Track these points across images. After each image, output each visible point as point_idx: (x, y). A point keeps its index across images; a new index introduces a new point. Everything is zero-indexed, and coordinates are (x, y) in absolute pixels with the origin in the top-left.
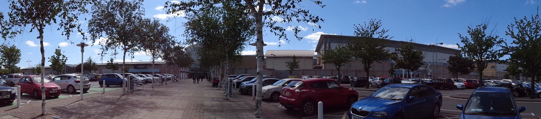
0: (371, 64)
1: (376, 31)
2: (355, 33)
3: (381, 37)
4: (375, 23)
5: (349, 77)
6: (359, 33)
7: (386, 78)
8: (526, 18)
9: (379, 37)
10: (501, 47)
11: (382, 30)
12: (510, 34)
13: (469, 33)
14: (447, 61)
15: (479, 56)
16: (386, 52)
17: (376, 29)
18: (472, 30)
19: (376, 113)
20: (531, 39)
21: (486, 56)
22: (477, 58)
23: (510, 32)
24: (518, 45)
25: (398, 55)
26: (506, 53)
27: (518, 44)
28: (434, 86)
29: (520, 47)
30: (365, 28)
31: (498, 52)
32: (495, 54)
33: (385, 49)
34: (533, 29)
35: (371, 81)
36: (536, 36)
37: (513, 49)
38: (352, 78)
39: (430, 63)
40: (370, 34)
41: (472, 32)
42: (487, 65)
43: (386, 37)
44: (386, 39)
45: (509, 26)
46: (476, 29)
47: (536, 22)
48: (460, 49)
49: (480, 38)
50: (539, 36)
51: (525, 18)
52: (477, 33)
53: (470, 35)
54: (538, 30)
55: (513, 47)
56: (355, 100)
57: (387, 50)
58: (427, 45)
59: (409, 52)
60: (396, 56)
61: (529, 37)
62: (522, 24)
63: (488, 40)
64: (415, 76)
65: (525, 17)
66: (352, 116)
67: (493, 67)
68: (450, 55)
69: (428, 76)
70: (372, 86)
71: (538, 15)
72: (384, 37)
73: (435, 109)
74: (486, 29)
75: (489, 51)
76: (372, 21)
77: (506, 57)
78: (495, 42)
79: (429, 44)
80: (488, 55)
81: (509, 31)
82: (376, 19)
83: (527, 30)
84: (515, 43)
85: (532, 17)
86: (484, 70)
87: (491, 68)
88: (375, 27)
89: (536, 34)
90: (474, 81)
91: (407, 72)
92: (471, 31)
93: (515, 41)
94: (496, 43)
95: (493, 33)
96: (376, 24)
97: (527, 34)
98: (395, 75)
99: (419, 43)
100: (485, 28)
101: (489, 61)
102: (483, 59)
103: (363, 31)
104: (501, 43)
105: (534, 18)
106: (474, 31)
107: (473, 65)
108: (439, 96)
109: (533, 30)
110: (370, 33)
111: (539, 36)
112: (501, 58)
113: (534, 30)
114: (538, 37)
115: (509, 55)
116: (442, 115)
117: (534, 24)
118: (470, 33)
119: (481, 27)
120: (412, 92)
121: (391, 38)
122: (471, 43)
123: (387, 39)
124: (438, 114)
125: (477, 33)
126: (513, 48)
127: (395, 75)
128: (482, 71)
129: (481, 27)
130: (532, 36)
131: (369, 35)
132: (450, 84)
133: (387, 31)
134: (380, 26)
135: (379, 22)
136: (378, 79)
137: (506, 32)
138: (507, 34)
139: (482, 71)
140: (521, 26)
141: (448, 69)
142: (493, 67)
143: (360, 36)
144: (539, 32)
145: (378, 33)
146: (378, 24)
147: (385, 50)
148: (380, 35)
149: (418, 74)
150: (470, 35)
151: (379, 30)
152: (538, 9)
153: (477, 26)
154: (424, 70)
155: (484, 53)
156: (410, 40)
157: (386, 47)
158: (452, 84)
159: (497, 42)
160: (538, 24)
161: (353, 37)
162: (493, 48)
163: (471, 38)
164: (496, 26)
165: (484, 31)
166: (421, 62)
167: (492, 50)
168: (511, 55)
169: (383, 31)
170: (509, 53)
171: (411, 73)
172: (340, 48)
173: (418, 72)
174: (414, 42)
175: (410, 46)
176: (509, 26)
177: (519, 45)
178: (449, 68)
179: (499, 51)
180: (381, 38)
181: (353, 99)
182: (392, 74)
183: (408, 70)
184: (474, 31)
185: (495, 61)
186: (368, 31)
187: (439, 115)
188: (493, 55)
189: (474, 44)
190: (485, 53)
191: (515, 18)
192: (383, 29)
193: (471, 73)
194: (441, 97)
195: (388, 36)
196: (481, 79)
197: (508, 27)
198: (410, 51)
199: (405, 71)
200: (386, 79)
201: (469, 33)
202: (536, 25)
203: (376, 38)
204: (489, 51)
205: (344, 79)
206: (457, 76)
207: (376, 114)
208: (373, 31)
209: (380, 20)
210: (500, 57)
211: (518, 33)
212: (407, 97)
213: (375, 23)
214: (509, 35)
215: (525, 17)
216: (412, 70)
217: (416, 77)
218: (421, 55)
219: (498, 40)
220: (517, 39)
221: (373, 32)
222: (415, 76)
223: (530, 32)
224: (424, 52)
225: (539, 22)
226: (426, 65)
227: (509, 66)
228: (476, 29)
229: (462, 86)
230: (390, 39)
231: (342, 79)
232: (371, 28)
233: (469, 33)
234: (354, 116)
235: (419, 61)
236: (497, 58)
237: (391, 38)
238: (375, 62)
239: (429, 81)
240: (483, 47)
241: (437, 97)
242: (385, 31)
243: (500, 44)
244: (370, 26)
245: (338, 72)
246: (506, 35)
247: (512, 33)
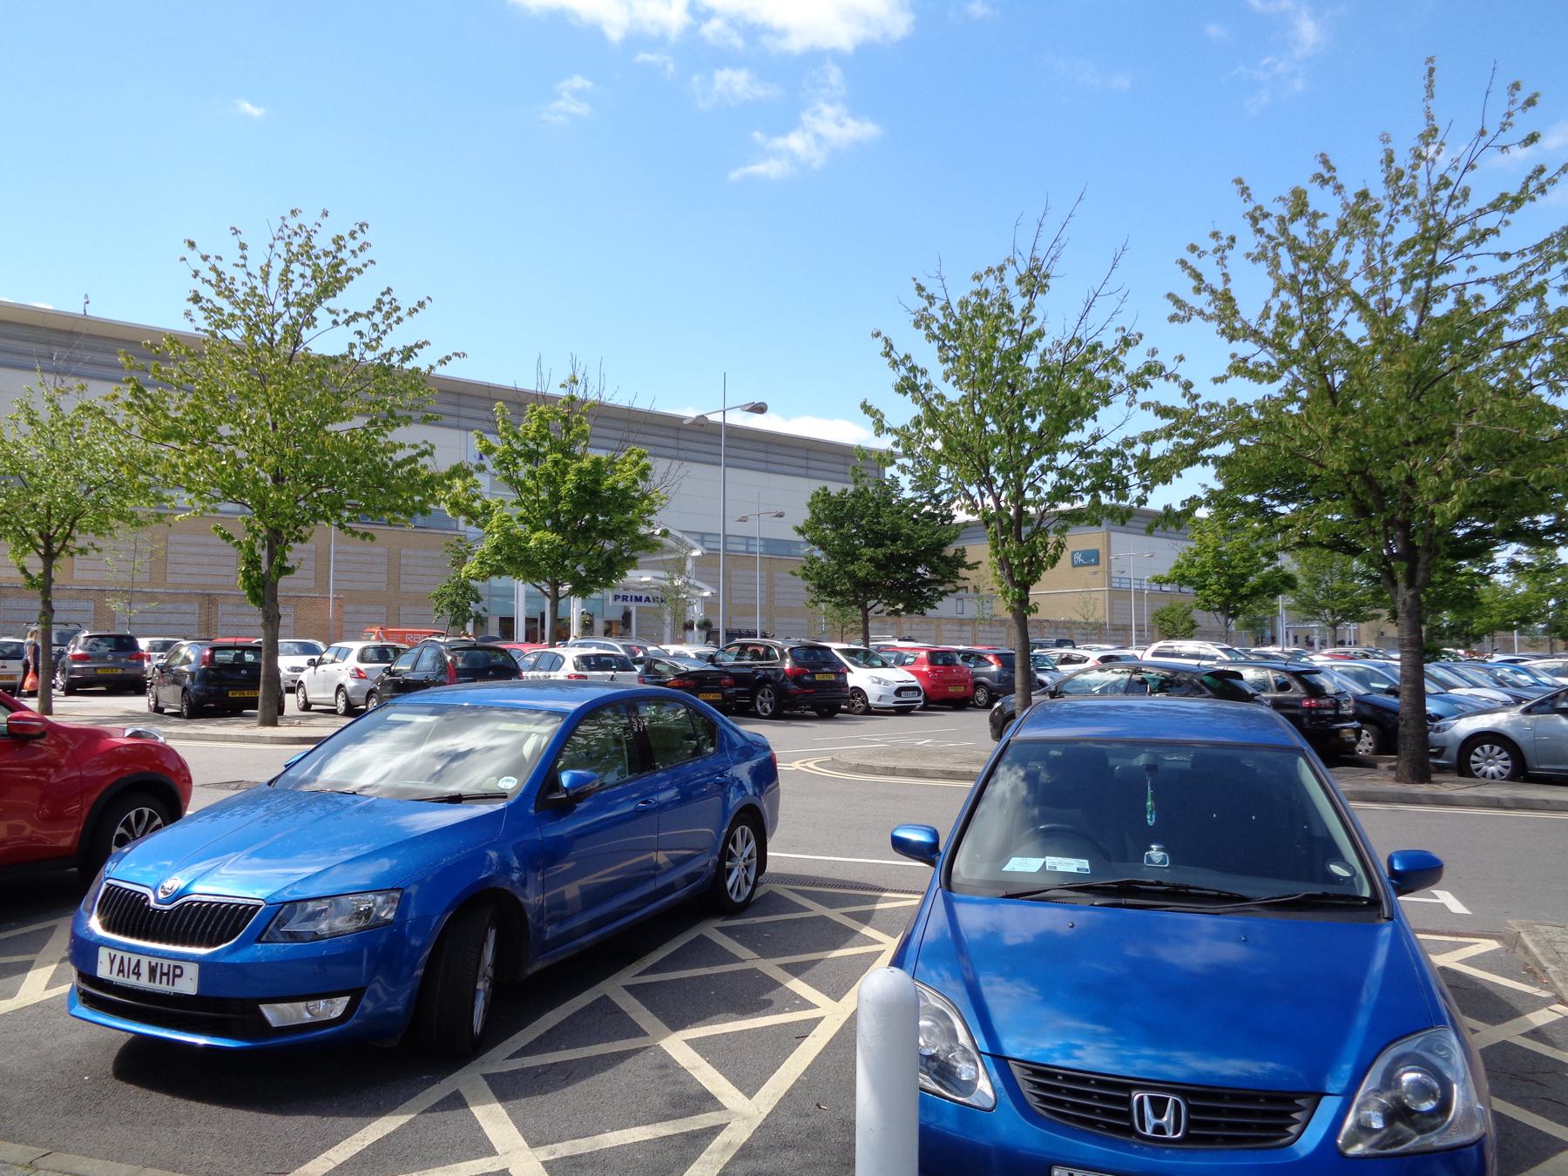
0: (297, 545)
1: (329, 303)
2: (194, 308)
3: (368, 346)
4: (322, 242)
5: (143, 643)
6: (228, 308)
7: (414, 646)
8: (1331, 168)
9: (352, 346)
10: (1151, 412)
11: (380, 301)
12: (1201, 313)
13: (928, 327)
14: (801, 525)
15: (1002, 489)
16: (413, 459)
17: (326, 291)
18: (942, 309)
19: (311, 906)
20: (1383, 321)
21: (1054, 487)
22: (989, 501)
23: (1206, 296)
24: (1275, 389)
25: (476, 485)
26: (1191, 457)
27: (1273, 378)
28: (717, 697)
29: (1291, 396)
30: (240, 275)
31: (1138, 449)
32: (1115, 462)
33: (398, 435)
34: (1400, 253)
35: (302, 670)
36: (1424, 301)
37: (1237, 420)
38: (166, 647)
39: (702, 537)
40: (285, 326)
41: (942, 321)
42: (1060, 546)
43: (408, 353)
44: (408, 365)
45: (1193, 248)
46: (974, 299)
47: (1422, 193)
48: (885, 443)
49: (1006, 356)
50: (1452, 296)
51: (1321, 169)
52: (979, 322)
53: (935, 345)
54: (1442, 256)
55: (1240, 403)
56: (159, 821)
57: (415, 446)
58: (680, 419)
59: (556, 463)
60: (465, 489)
61: (1372, 319)
62: (1299, 229)
63: (1066, 367)
64: (599, 625)
65: (1326, 162)
66: (104, 954)
67: (1091, 558)
68: (816, 485)
69: (689, 626)
70: (307, 706)
71: (1433, 131)
72: (393, 351)
73: (731, 856)
74: (1043, 288)
75: (1069, 448)
76: (293, 223)
77: (1197, 481)
78: (1117, 379)
79: (690, 413)
80: (1063, 472)
81: (1198, 290)
82: (326, 214)
83: (1344, 264)
84: (1255, 375)
85: (1389, 159)
86: (1045, 575)
87: (1074, 566)
88: (317, 271)
89: (1420, 284)
90: (967, 656)
91: (548, 602)
92: (939, 315)
93: (1245, 360)
94: (1125, 382)
95: (1097, 317)
96: (332, 248)
97: (1343, 288)
98: (480, 621)
99: (624, 403)
100: (1035, 282)
101: (1076, 517)
102: (1033, 503)
103: (229, 294)
104: (1146, 385)
105: (1403, 160)
106: (957, 312)
107: (949, 551)
108: (753, 763)
109: (1402, 259)
110: (286, 318)
111: (1452, 296)
112: (1159, 488)
113: (1406, 258)
114: (1439, 310)
115: (1211, 470)
116: (781, 889)
117: (1406, 210)
118: (935, 327)
119: (1011, 276)
120: (581, 741)
121: (442, 362)
122: (941, 397)
123: (417, 370)
124: (756, 885)
125: (979, 322)
126: (1239, 410)
127: (480, 621)
128: (1027, 589)
129: (1011, 276)
130: (1386, 304)
131: (278, 327)
132: (818, 677)
133: (413, 311)
134: (359, 271)
135: (353, 235)
136: (349, 651)
137: (1170, 296)
138: (1182, 312)
139: (1025, 586)
140: (1294, 245)
141: (806, 577)
142: (1091, 558)
143: (236, 334)
144: (1452, 268)
145: (347, 323)
146: (345, 254)
147: (402, 446)
148: (360, 333)
149: (618, 616)
150: (935, 345)
151: (355, 297)
152: (1430, 86)
153: (977, 277)
154: (663, 589)
155: (1036, 464)
156: (565, 376)
157: (408, 420)
158: (833, 678)
159: (1130, 378)
160: (1439, 208)
161: (175, 339)
162: (1095, 418)
163: (946, 360)
164: (1116, 260)
165: (1031, 306)
166: (643, 530)
167: (1095, 439)
168: (1221, 463)
169: (387, 309)
170: (1206, 452)
171: (575, 609)
172: (57, 409)
173: (619, 602)
174: (593, 396)
175: (566, 419)
176: (1193, 248)
177: (1280, 384)
178: (810, 572)
179: (1149, 438)
180: (369, 356)
181: (139, 816)
182: (460, 616)
183: (555, 585)
184: (957, 312)
185: (1123, 517)
186: (262, 302)
187: (760, 892)
188: (1105, 476)
189: (964, 399)
190: (1044, 460)
191: (1239, 181)
192: (389, 291)
193: (937, 604)
194: (766, 773)
195: (420, 346)
196: (1026, 646)
197: (1183, 263)
198: (567, 454)
199: (528, 596)
200: (416, 651)
201: (928, 327)
202: (1424, 219)
203: (334, 360)
204: (1069, 448)
205: (102, 657)
206: (866, 620)
207: (313, 916)
208: (308, 305)
209: (362, 226)
210: (1154, 484)
211: (1276, 292)
212: (544, 778)
213: (322, 242)
214: (1195, 318)
215: (1326, 162)
216: (582, 588)
217: (607, 633)
218: (641, 484)
219: (1134, 360)
220: (1264, 342)
221: (312, 307)
222: (599, 625)
223: (1371, 272)
224: (659, 466)
225: (1446, 183)
226: (672, 551)
227: (1193, 545)
228: (974, 299)
229: (899, 692)
230: (440, 371)
231: (77, 659)
232: (286, 282)
233: (922, 332)
234: (119, 954)
235: (630, 523)
236: (1135, 492)
237: (442, 362)
238: (326, 534)
239: (699, 656)
240: (1028, 422)
241: (742, 771)
242: (398, 309)
243: (1140, 390)
244: (278, 266)
245: (38, 605)
246: (1173, 318)
247: (1227, 299)
